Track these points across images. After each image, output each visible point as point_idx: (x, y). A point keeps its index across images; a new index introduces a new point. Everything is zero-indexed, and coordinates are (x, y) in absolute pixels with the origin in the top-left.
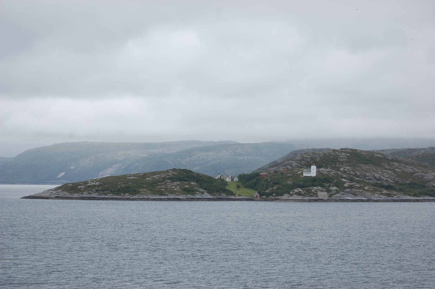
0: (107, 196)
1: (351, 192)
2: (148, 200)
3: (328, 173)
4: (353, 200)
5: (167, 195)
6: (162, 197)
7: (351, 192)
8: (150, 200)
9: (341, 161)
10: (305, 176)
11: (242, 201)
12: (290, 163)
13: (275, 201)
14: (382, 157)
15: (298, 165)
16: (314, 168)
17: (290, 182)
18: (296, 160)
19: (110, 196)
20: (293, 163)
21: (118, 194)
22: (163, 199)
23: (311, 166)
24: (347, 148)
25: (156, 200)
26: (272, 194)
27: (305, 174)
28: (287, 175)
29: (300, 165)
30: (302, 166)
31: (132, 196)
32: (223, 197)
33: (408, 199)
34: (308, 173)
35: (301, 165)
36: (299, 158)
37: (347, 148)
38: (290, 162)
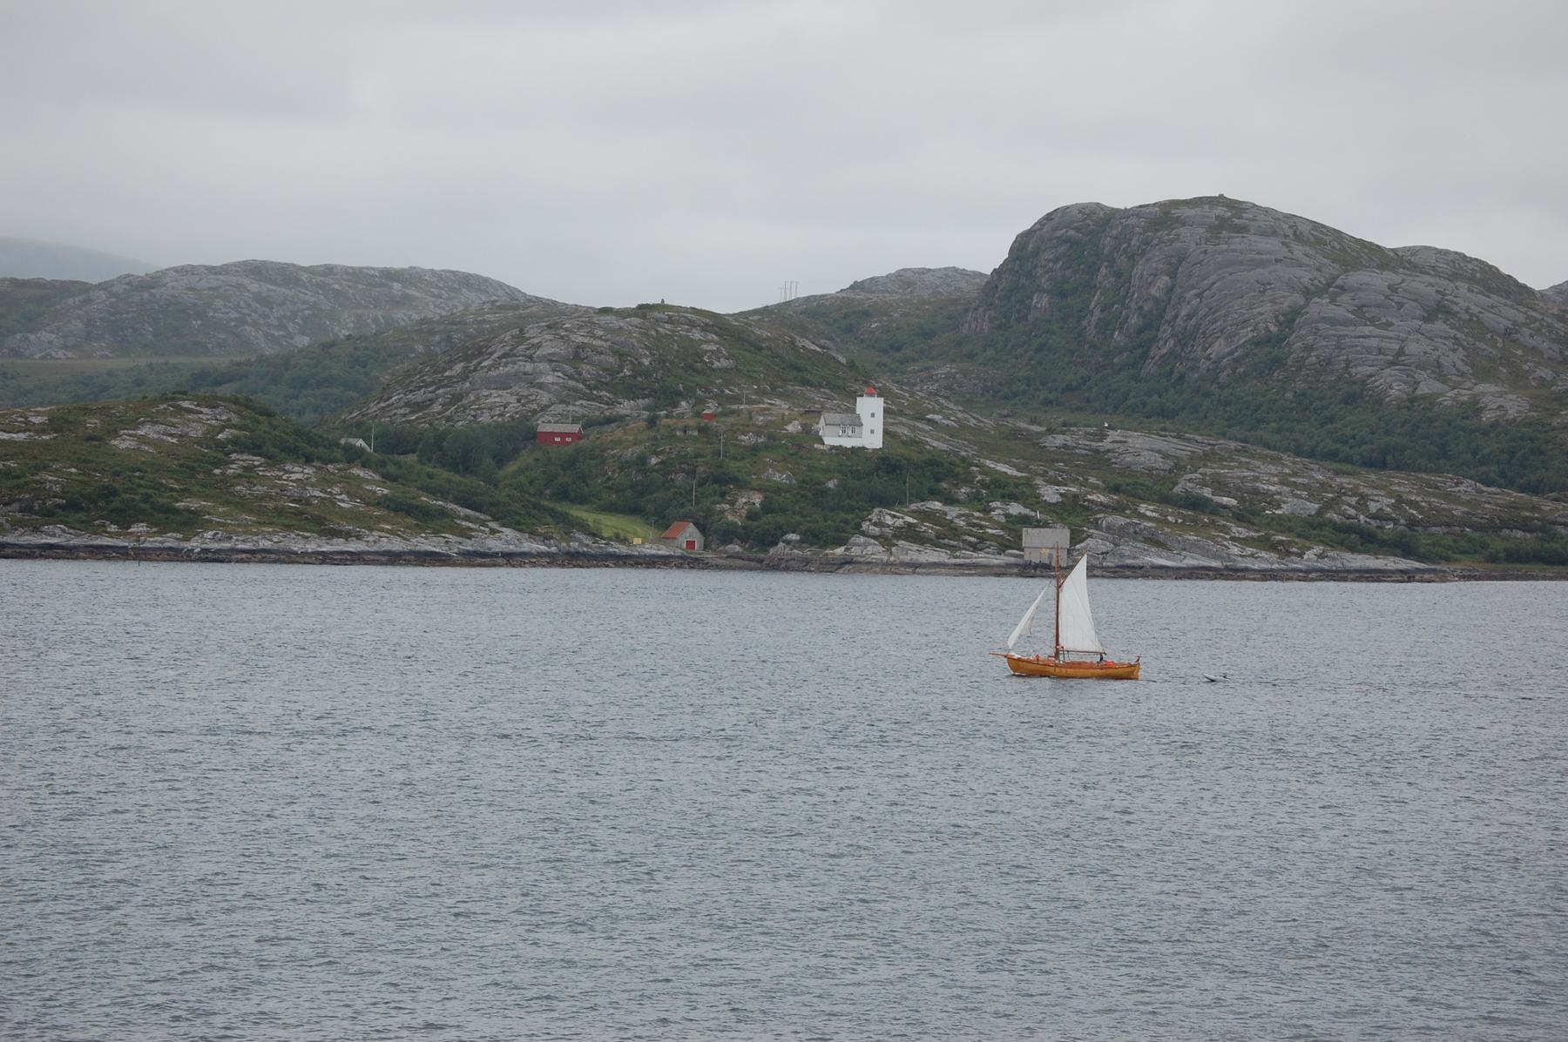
0: (48, 534)
1: (1136, 533)
2: (298, 559)
3: (1172, 445)
4: (1182, 572)
5: (347, 536)
6: (339, 545)
7: (1136, 533)
8: (305, 563)
9: (718, 368)
10: (833, 447)
11: (1345, 579)
12: (525, 374)
13: (841, 571)
14: (817, 352)
15: (572, 383)
16: (871, 408)
17: (782, 473)
18: (544, 356)
19: (57, 536)
20: (541, 373)
21: (87, 526)
22: (366, 557)
23: (858, 399)
24: (663, 301)
25: (364, 560)
26: (779, 532)
27: (830, 439)
28: (736, 439)
29: (581, 386)
30: (591, 390)
31: (180, 536)
32: (585, 549)
33: (106, 543)
34: (850, 434)
35: (584, 381)
36: (558, 350)
37: (663, 301)
38: (522, 369)
